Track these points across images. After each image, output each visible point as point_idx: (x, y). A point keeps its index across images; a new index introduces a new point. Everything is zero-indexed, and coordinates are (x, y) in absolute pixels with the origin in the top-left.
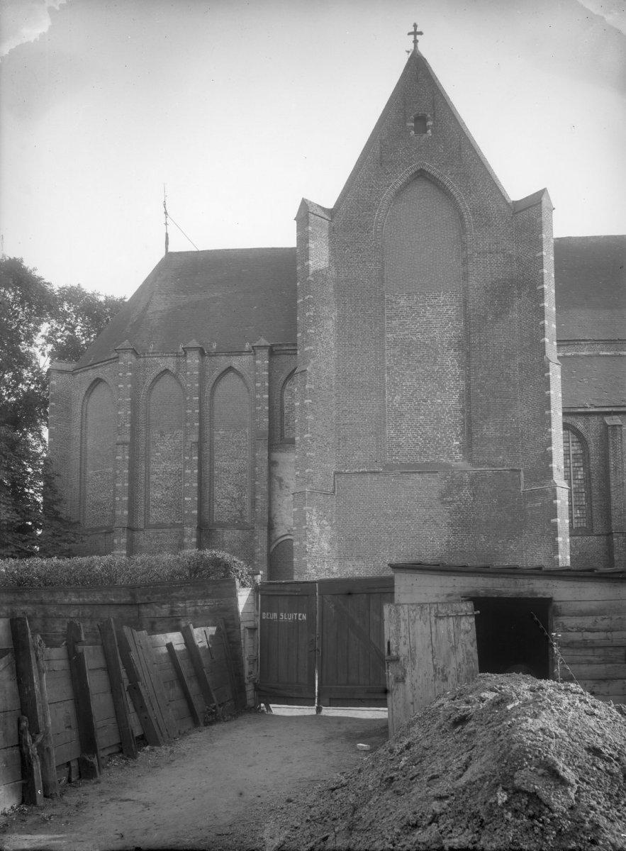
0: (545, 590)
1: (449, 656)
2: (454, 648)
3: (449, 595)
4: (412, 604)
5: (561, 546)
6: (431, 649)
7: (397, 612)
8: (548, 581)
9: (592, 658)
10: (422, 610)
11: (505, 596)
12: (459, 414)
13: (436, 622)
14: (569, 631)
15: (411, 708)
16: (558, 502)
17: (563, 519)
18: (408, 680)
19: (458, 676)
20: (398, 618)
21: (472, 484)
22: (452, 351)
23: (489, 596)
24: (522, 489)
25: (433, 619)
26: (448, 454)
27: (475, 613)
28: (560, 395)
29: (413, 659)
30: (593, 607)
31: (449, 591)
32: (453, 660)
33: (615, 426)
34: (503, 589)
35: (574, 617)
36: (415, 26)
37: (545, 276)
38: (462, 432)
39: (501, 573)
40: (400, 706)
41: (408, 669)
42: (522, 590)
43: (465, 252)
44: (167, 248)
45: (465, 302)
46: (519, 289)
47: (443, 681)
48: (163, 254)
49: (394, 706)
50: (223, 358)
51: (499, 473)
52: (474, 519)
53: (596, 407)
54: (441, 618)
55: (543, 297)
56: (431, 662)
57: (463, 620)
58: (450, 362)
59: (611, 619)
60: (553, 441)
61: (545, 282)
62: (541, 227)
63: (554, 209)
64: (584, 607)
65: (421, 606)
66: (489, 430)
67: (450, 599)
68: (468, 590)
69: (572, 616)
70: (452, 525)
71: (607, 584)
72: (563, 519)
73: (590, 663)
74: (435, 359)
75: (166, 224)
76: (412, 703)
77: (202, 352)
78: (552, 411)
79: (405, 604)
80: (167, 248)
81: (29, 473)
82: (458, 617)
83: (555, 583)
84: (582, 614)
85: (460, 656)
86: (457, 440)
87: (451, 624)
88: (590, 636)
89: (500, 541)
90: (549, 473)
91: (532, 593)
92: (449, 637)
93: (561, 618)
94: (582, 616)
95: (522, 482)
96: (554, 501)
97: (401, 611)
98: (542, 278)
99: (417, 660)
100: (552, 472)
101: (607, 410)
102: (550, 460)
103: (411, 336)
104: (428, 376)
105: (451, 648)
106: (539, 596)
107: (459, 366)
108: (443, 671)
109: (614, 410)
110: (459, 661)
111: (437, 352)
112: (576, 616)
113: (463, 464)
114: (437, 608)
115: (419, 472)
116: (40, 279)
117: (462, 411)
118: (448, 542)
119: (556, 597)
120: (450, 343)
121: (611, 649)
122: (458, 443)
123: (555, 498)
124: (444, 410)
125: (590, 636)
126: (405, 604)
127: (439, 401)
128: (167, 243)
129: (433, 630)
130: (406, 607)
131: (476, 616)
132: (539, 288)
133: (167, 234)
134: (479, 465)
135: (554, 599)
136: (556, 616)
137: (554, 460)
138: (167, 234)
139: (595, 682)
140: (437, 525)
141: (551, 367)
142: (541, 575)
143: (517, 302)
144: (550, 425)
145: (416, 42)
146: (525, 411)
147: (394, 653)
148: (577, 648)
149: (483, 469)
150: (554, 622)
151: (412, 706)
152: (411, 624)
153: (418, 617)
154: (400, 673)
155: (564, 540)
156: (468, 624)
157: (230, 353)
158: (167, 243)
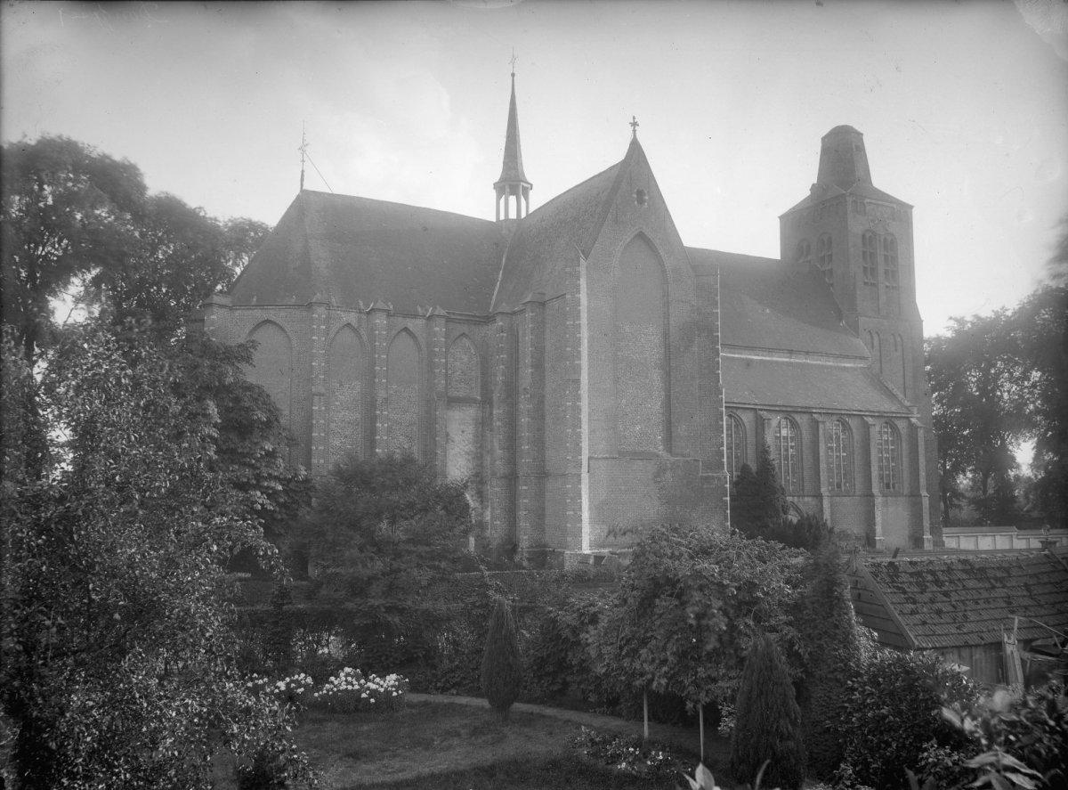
12: (661, 416)
36: (634, 118)
44: (302, 185)
48: (298, 192)
50: (400, 318)
58: (656, 377)
75: (303, 161)
77: (448, 320)
80: (302, 185)
81: (116, 620)
113: (665, 455)
116: (60, 137)
128: (302, 180)
133: (303, 171)
134: (677, 455)
138: (303, 171)
145: (634, 131)
157: (405, 316)
158: (302, 180)
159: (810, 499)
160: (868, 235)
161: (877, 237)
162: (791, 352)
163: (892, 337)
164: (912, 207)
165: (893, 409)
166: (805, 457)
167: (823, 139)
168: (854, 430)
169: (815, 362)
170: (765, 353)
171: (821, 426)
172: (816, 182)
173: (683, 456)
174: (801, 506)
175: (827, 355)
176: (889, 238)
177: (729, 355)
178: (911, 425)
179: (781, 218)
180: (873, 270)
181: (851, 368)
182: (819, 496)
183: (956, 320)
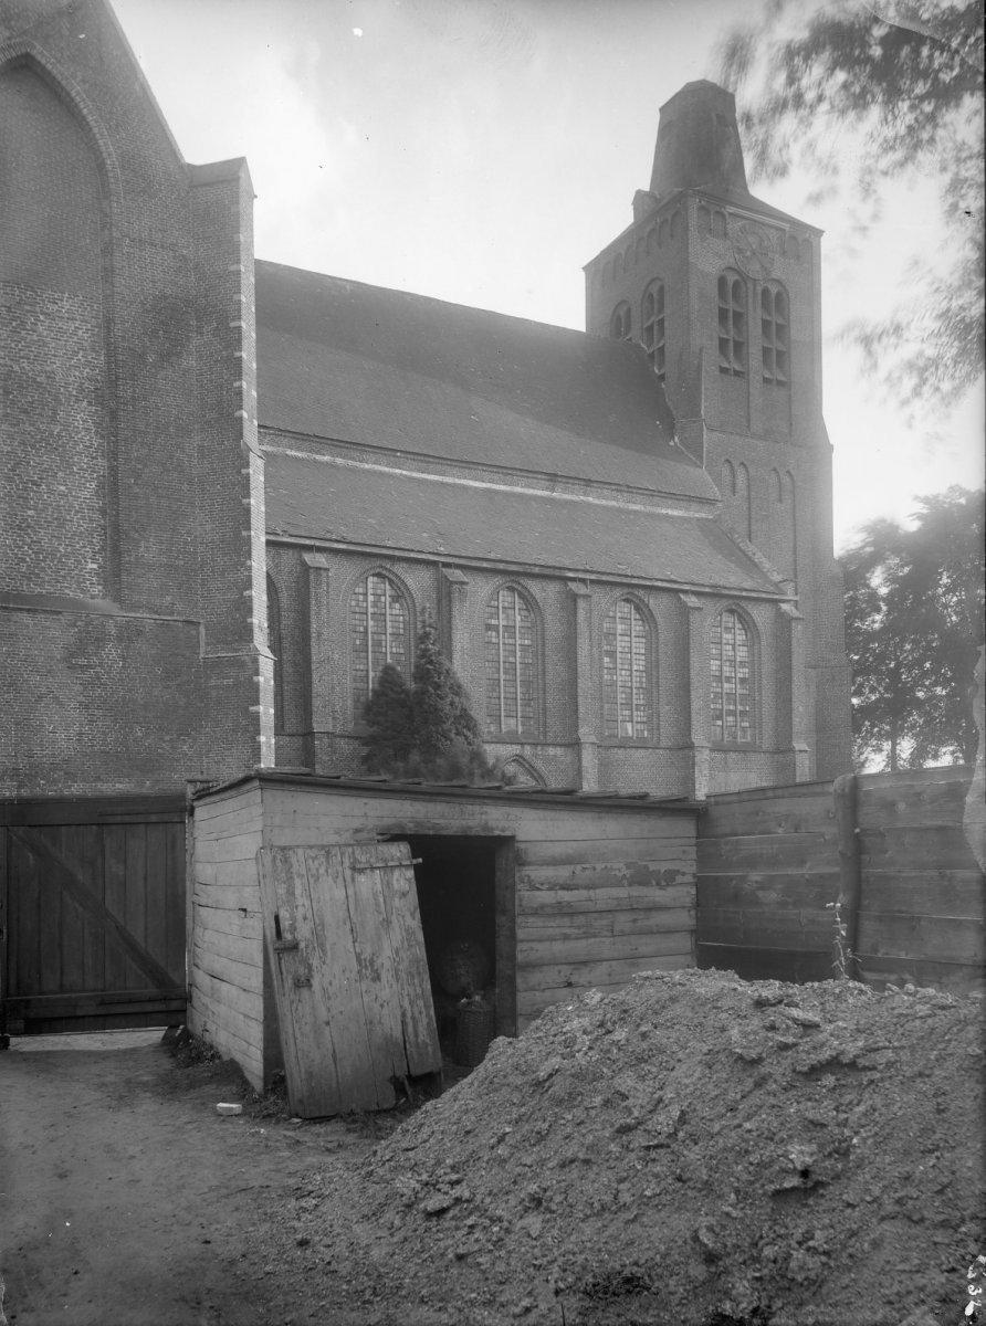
0: (502, 824)
1: (379, 939)
2: (387, 922)
3: (357, 831)
4: (311, 847)
5: (264, 750)
6: (348, 927)
7: (286, 861)
8: (507, 809)
9: (568, 931)
10: (327, 858)
11: (444, 833)
12: (96, 516)
13: (353, 880)
14: (538, 889)
15: (327, 1032)
16: (261, 679)
17: (266, 708)
18: (315, 982)
19: (397, 971)
20: (289, 871)
21: (120, 639)
22: (85, 403)
23: (421, 832)
24: (202, 655)
25: (348, 873)
26: (79, 583)
27: (415, 862)
28: (263, 509)
29: (322, 945)
30: (571, 851)
31: (357, 823)
32: (386, 945)
33: (320, 569)
34: (441, 821)
35: (545, 867)
37: (243, 306)
38: (103, 549)
39: (438, 794)
40: (308, 1028)
41: (315, 962)
42: (471, 823)
43: (106, 232)
45: (108, 323)
46: (198, 319)
47: (374, 980)
49: (297, 1030)
51: (165, 625)
52: (124, 698)
53: (291, 536)
54: (361, 871)
55: (239, 341)
56: (352, 950)
57: (397, 873)
59: (595, 869)
60: (254, 582)
61: (244, 317)
62: (238, 222)
63: (256, 197)
64: (558, 850)
65: (327, 850)
66: (149, 550)
67: (359, 839)
68: (388, 822)
69: (542, 865)
70: (87, 707)
71: (590, 815)
72: (266, 708)
73: (566, 937)
74: (55, 413)
76: (328, 1023)
78: (252, 533)
79: (298, 846)
82: (387, 868)
83: (516, 811)
84: (555, 862)
85: (397, 936)
86: (94, 561)
87: (378, 881)
88: (566, 896)
89: (167, 738)
90: (246, 633)
91: (486, 827)
92: (377, 905)
93: (527, 868)
94: (554, 865)
95: (202, 644)
96: (255, 678)
97: (294, 860)
98: (239, 310)
99: (328, 947)
100: (251, 630)
101: (308, 542)
102: (250, 611)
103: (9, 363)
104: (42, 439)
105: (381, 923)
106: (497, 833)
107: (97, 433)
108: (372, 962)
109: (318, 543)
110: (395, 944)
111: (56, 399)
112: (548, 865)
114: (353, 853)
115: (28, 610)
117: (103, 512)
118: (80, 734)
119: (520, 836)
120: (81, 389)
121: (595, 915)
122: (95, 566)
123: (257, 673)
124: (71, 506)
125: (566, 896)
126: (298, 846)
127: (63, 488)
129: (350, 892)
130: (300, 851)
131: (417, 868)
132: (232, 324)
134: (134, 607)
135: (517, 838)
136: (520, 865)
137: (255, 613)
139: (573, 967)
140: (61, 705)
141: (251, 461)
142: (500, 798)
143: (196, 341)
144: (249, 556)
146: (208, 527)
147: (288, 936)
148: (549, 915)
149: (139, 615)
150: (517, 875)
151: (328, 1028)
152: (312, 881)
153: (322, 871)
154: (302, 971)
155: (267, 739)
156: (404, 880)
159: (559, 751)
160: (732, 278)
161: (750, 285)
162: (553, 478)
163: (773, 475)
164: (819, 233)
165: (746, 585)
166: (549, 667)
167: (662, 110)
168: (660, 620)
169: (604, 502)
170: (496, 477)
171: (581, 604)
172: (646, 187)
173: (151, 610)
174: (539, 764)
175: (630, 489)
176: (774, 290)
177: (415, 475)
178: (780, 615)
179: (585, 268)
180: (738, 346)
181: (679, 517)
182: (575, 745)
183: (926, 500)
